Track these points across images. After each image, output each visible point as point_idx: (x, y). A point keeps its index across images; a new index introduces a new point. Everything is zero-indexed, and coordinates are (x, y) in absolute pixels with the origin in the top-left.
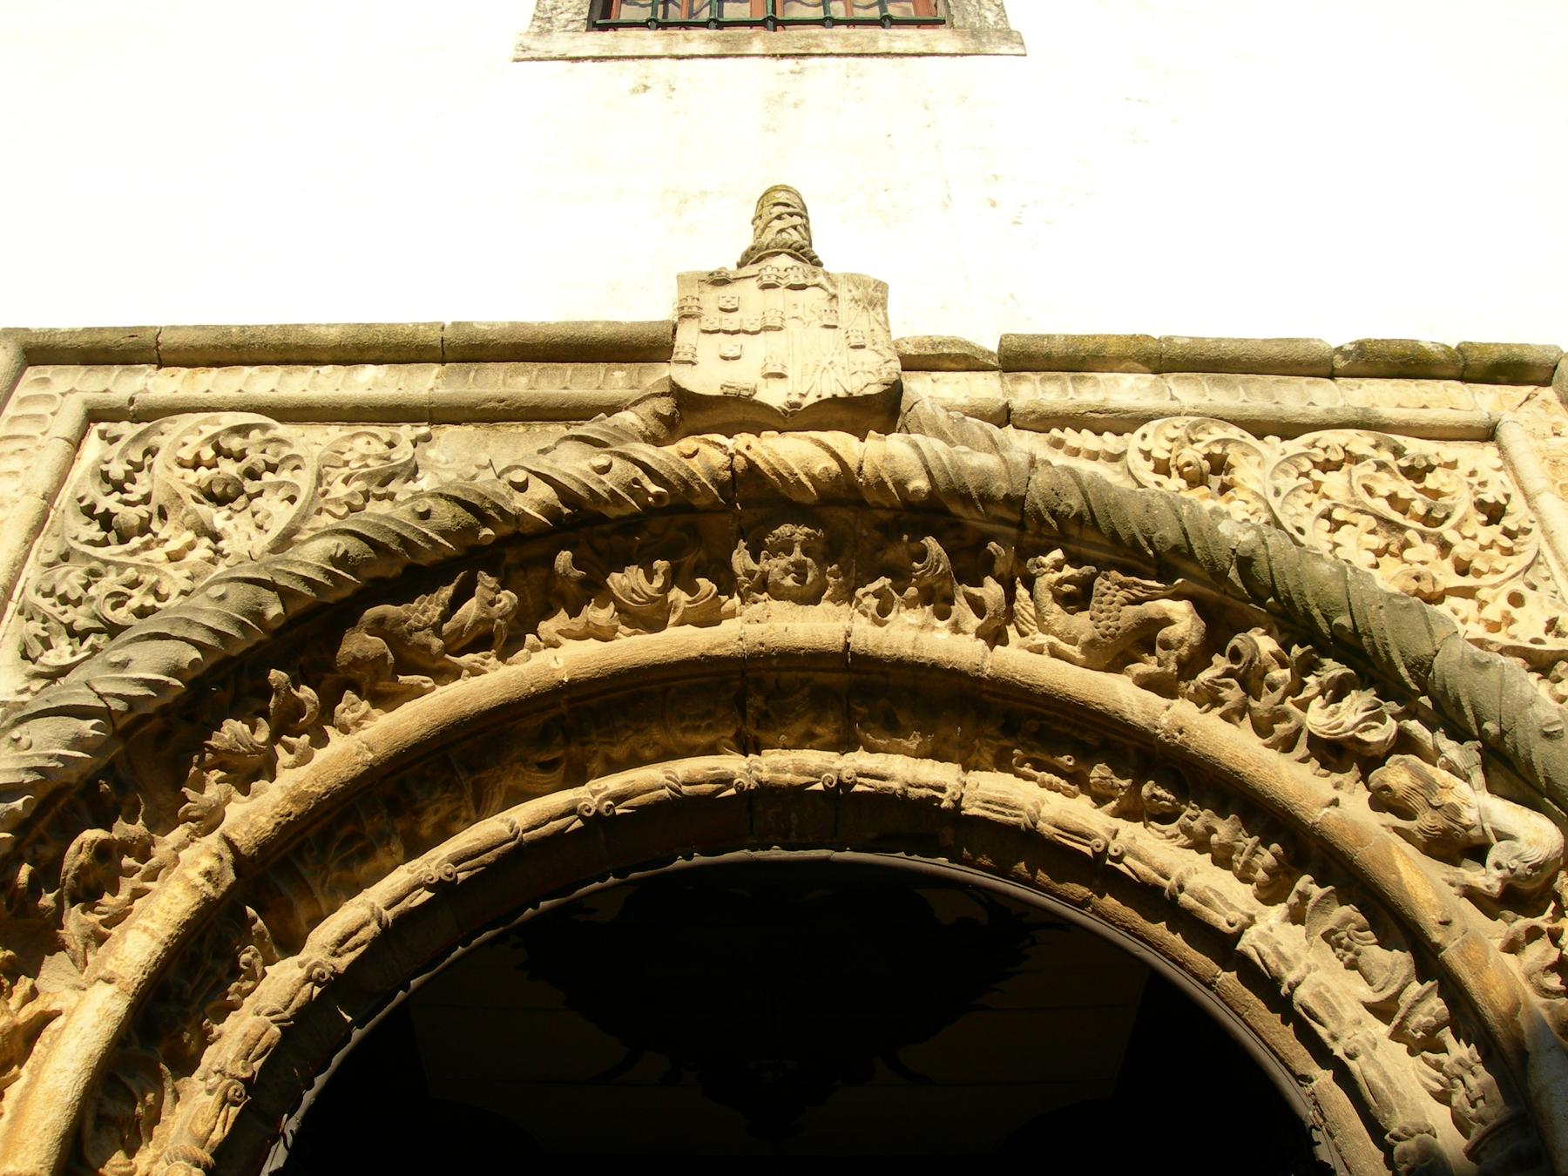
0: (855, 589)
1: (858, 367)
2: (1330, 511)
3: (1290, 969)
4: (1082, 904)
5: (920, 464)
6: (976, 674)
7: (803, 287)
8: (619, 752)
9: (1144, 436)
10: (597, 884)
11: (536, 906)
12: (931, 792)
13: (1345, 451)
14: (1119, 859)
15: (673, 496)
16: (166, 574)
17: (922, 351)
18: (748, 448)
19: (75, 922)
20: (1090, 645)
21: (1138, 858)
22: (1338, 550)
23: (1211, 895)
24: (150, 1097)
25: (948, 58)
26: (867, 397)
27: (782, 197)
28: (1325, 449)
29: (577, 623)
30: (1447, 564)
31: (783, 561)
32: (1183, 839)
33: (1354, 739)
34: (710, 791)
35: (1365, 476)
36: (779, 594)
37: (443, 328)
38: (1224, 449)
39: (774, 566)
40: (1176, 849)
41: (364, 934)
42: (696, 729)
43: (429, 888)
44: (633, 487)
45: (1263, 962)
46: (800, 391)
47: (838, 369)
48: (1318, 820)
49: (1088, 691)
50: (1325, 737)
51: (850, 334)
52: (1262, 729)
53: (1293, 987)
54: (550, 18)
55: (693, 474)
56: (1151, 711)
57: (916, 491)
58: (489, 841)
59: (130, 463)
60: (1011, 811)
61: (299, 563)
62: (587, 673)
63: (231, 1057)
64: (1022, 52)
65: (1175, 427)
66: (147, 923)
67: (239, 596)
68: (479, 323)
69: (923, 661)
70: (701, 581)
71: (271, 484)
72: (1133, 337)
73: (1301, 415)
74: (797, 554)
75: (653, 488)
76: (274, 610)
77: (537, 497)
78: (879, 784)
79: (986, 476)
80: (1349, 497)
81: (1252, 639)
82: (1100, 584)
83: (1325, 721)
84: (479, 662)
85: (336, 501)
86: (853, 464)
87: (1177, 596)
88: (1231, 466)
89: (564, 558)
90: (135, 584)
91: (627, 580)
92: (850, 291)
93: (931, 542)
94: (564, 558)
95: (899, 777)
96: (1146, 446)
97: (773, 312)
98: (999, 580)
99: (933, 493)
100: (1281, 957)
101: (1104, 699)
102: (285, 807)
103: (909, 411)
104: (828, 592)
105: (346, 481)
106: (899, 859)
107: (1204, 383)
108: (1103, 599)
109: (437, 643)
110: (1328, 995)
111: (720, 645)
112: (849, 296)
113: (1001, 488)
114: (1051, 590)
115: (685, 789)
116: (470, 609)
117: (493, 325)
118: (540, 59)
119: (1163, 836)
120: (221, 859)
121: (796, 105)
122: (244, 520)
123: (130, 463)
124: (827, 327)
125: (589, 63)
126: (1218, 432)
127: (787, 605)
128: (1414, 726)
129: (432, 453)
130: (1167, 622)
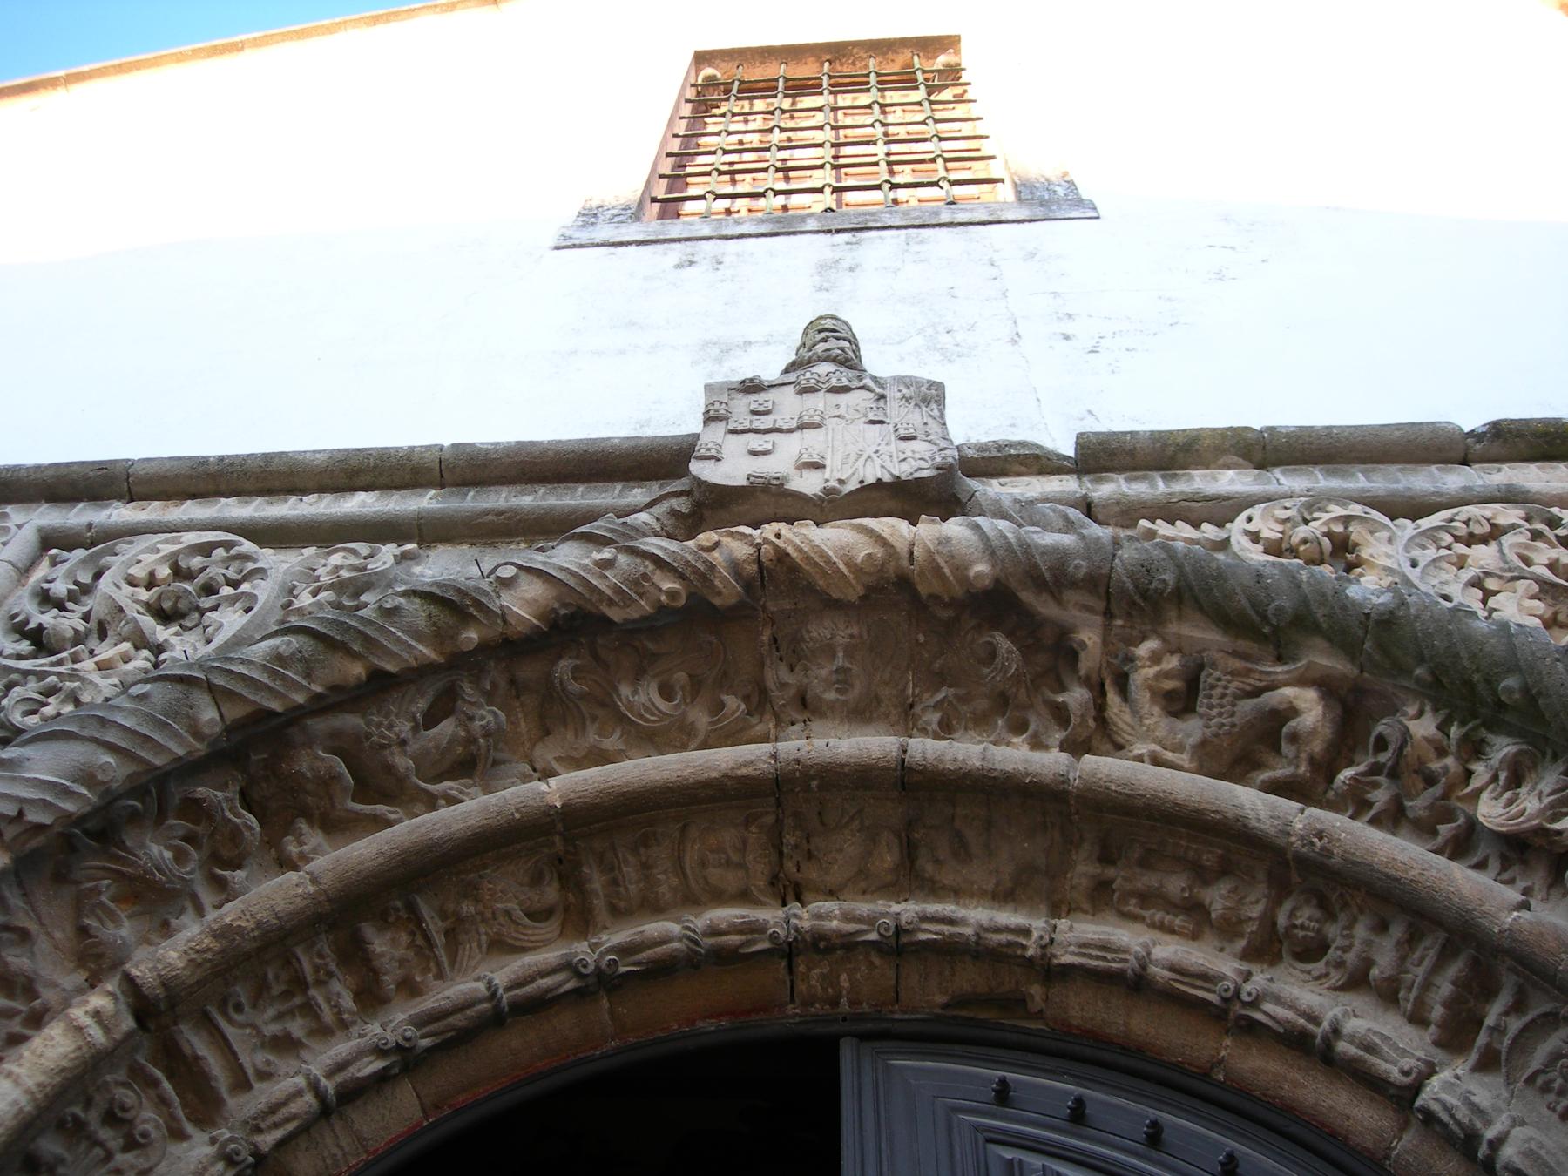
1: (909, 454)
3: (1488, 1123)
6: (1061, 787)
7: (845, 390)
9: (1250, 519)
12: (1011, 937)
13: (1491, 524)
14: (1255, 1004)
15: (690, 596)
16: (91, 682)
17: (986, 454)
18: (778, 536)
22: (1495, 615)
23: (1376, 1040)
25: (1015, 225)
27: (829, 324)
28: (1467, 523)
33: (1541, 831)
34: (738, 943)
35: (1520, 545)
37: (441, 450)
38: (1346, 528)
40: (1325, 992)
44: (639, 581)
45: (1452, 1116)
46: (840, 477)
47: (885, 457)
48: (1507, 926)
49: (1201, 797)
50: (1504, 829)
51: (899, 426)
53: (1496, 1144)
54: (595, 214)
56: (1281, 815)
57: (979, 575)
59: (76, 583)
60: (1114, 955)
61: (239, 661)
62: (584, 796)
64: (1095, 215)
65: (1286, 508)
68: (481, 444)
69: (995, 774)
72: (1230, 429)
73: (1433, 494)
74: (840, 660)
75: (668, 584)
77: (528, 596)
78: (947, 929)
80: (1502, 565)
81: (1400, 722)
83: (1502, 811)
84: (457, 790)
88: (1356, 545)
90: (51, 691)
92: (900, 391)
93: (1003, 643)
95: (972, 921)
96: (1252, 527)
97: (812, 412)
98: (1086, 682)
102: (202, 942)
103: (970, 500)
105: (315, 594)
107: (1316, 472)
108: (1213, 692)
110: (1542, 1152)
112: (899, 395)
114: (1150, 688)
117: (498, 443)
118: (581, 246)
119: (1308, 977)
121: (851, 269)
123: (76, 583)
124: (873, 422)
125: (633, 248)
126: (1337, 511)
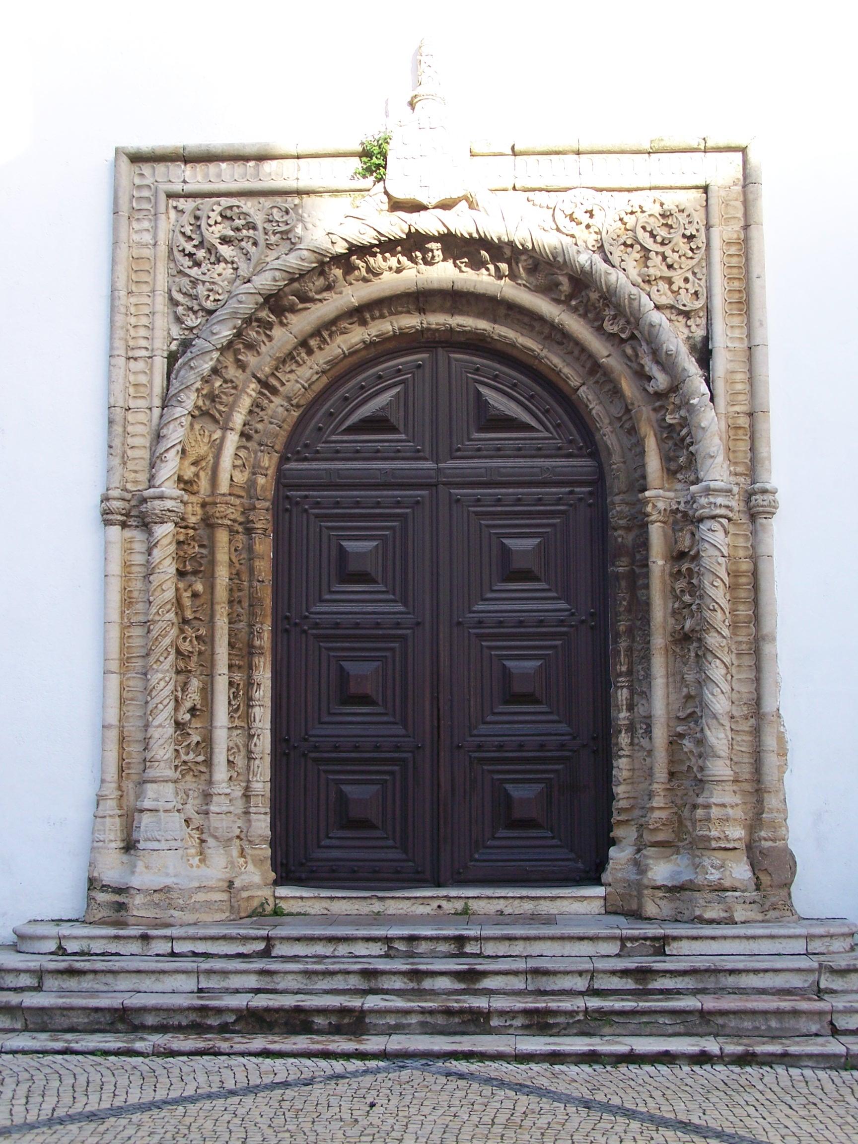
20: (536, 286)
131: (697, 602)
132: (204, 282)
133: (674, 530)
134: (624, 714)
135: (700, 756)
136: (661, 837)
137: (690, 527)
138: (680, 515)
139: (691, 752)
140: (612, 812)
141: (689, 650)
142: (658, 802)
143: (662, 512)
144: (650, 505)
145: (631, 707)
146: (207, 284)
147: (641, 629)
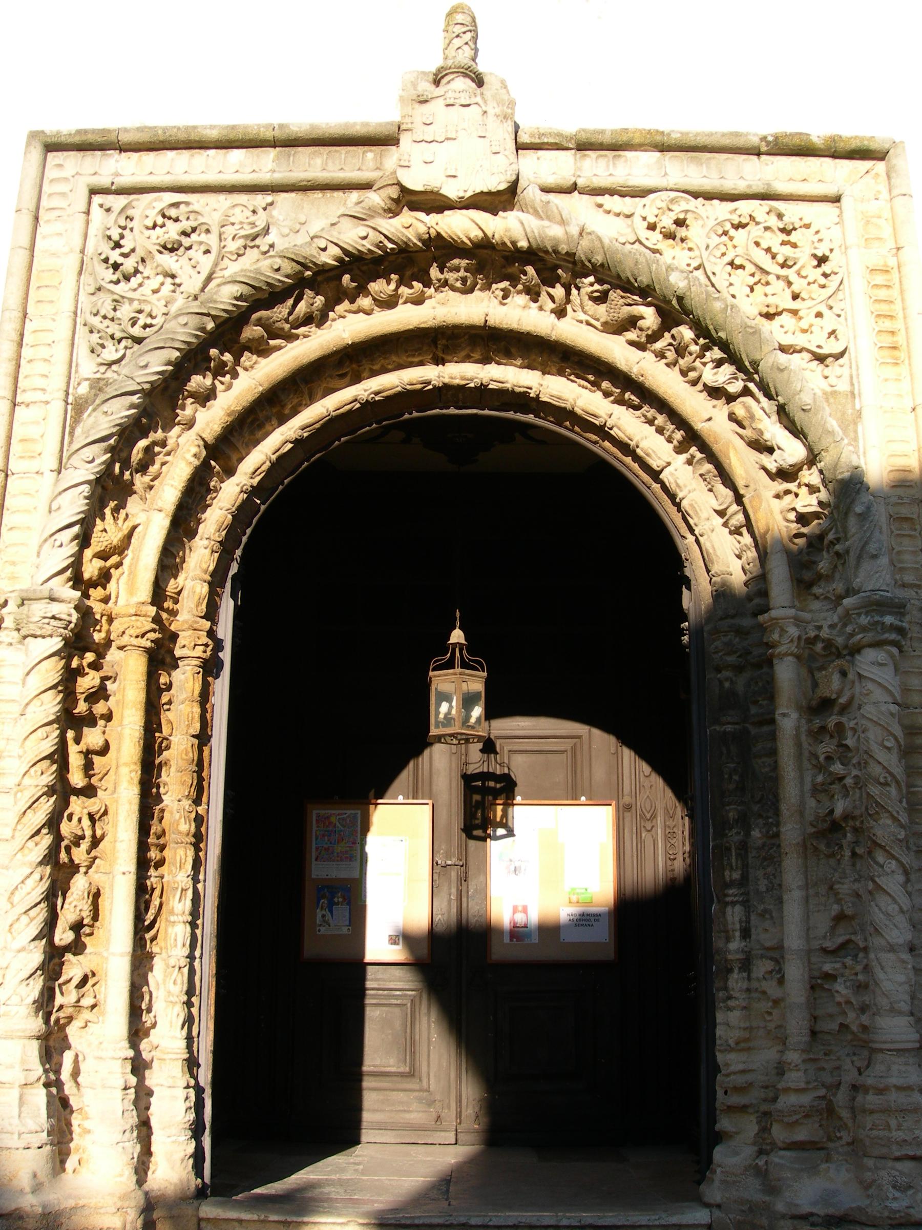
0: (492, 283)
2: (733, 261)
3: (681, 491)
4: (596, 443)
5: (523, 233)
7: (469, 105)
8: (376, 367)
10: (368, 428)
11: (339, 440)
14: (611, 429)
19: (140, 481)
20: (605, 324)
21: (619, 429)
22: (731, 287)
24: (181, 554)
26: (499, 191)
29: (354, 307)
30: (788, 294)
31: (455, 275)
32: (643, 419)
36: (453, 289)
39: (451, 276)
41: (264, 467)
42: (413, 356)
43: (291, 442)
52: (684, 373)
55: (409, 239)
58: (317, 419)
63: (213, 531)
66: (171, 482)
67: (194, 321)
70: (414, 283)
71: (196, 242)
75: (390, 246)
76: (210, 325)
77: (332, 254)
79: (557, 242)
82: (612, 295)
85: (231, 253)
86: (490, 235)
87: (649, 305)
89: (346, 278)
91: (378, 287)
94: (346, 278)
98: (563, 285)
99: (530, 247)
100: (678, 485)
101: (608, 357)
104: (478, 286)
106: (510, 415)
109: (287, 326)
111: (424, 323)
113: (563, 248)
115: (409, 387)
116: (302, 307)
120: (199, 446)
122: (184, 261)
127: (458, 294)
128: (751, 386)
129: (275, 213)
130: (642, 318)
131: (855, 772)
132: (131, 300)
133: (811, 672)
134: (735, 944)
135: (863, 1009)
136: (801, 1135)
137: (838, 662)
138: (819, 647)
139: (848, 1002)
140: (716, 1091)
141: (841, 847)
142: (794, 1078)
143: (795, 640)
144: (777, 631)
145: (746, 933)
146: (136, 303)
147: (760, 816)
